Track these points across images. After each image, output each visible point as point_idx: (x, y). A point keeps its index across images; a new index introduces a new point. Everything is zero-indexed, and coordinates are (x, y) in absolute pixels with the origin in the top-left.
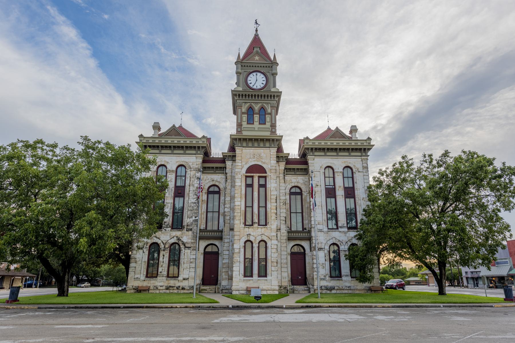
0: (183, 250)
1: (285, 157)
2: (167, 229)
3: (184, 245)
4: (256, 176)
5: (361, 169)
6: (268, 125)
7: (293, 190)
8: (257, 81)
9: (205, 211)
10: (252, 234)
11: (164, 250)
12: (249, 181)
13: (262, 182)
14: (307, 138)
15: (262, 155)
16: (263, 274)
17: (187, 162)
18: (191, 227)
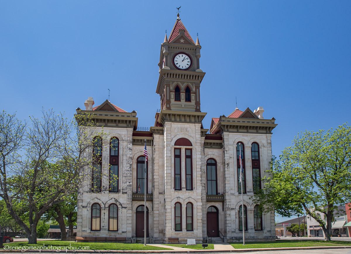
0: (121, 210)
1: (205, 132)
2: (106, 192)
3: (121, 206)
4: (183, 148)
5: (266, 144)
6: (193, 102)
7: (209, 162)
8: (182, 61)
9: (136, 178)
10: (181, 197)
11: (104, 209)
12: (177, 153)
13: (188, 154)
14: (224, 116)
15: (189, 129)
16: (190, 228)
17: (119, 135)
18: (125, 191)
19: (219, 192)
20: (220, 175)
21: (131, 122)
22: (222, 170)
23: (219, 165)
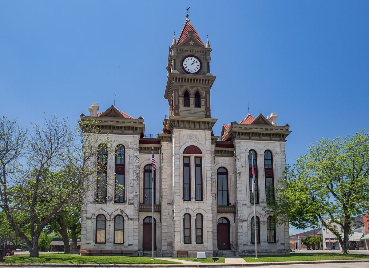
0: (127, 221)
1: (215, 139)
2: (111, 203)
3: (128, 217)
4: (193, 156)
5: (279, 152)
6: (203, 108)
7: (220, 171)
8: (191, 65)
9: (143, 188)
10: (190, 207)
11: (110, 221)
12: (187, 162)
13: (198, 162)
15: (198, 136)
16: (199, 241)
17: (126, 142)
18: (132, 202)
19: (230, 202)
20: (231, 184)
21: (138, 129)
22: (233, 179)
23: (230, 174)
